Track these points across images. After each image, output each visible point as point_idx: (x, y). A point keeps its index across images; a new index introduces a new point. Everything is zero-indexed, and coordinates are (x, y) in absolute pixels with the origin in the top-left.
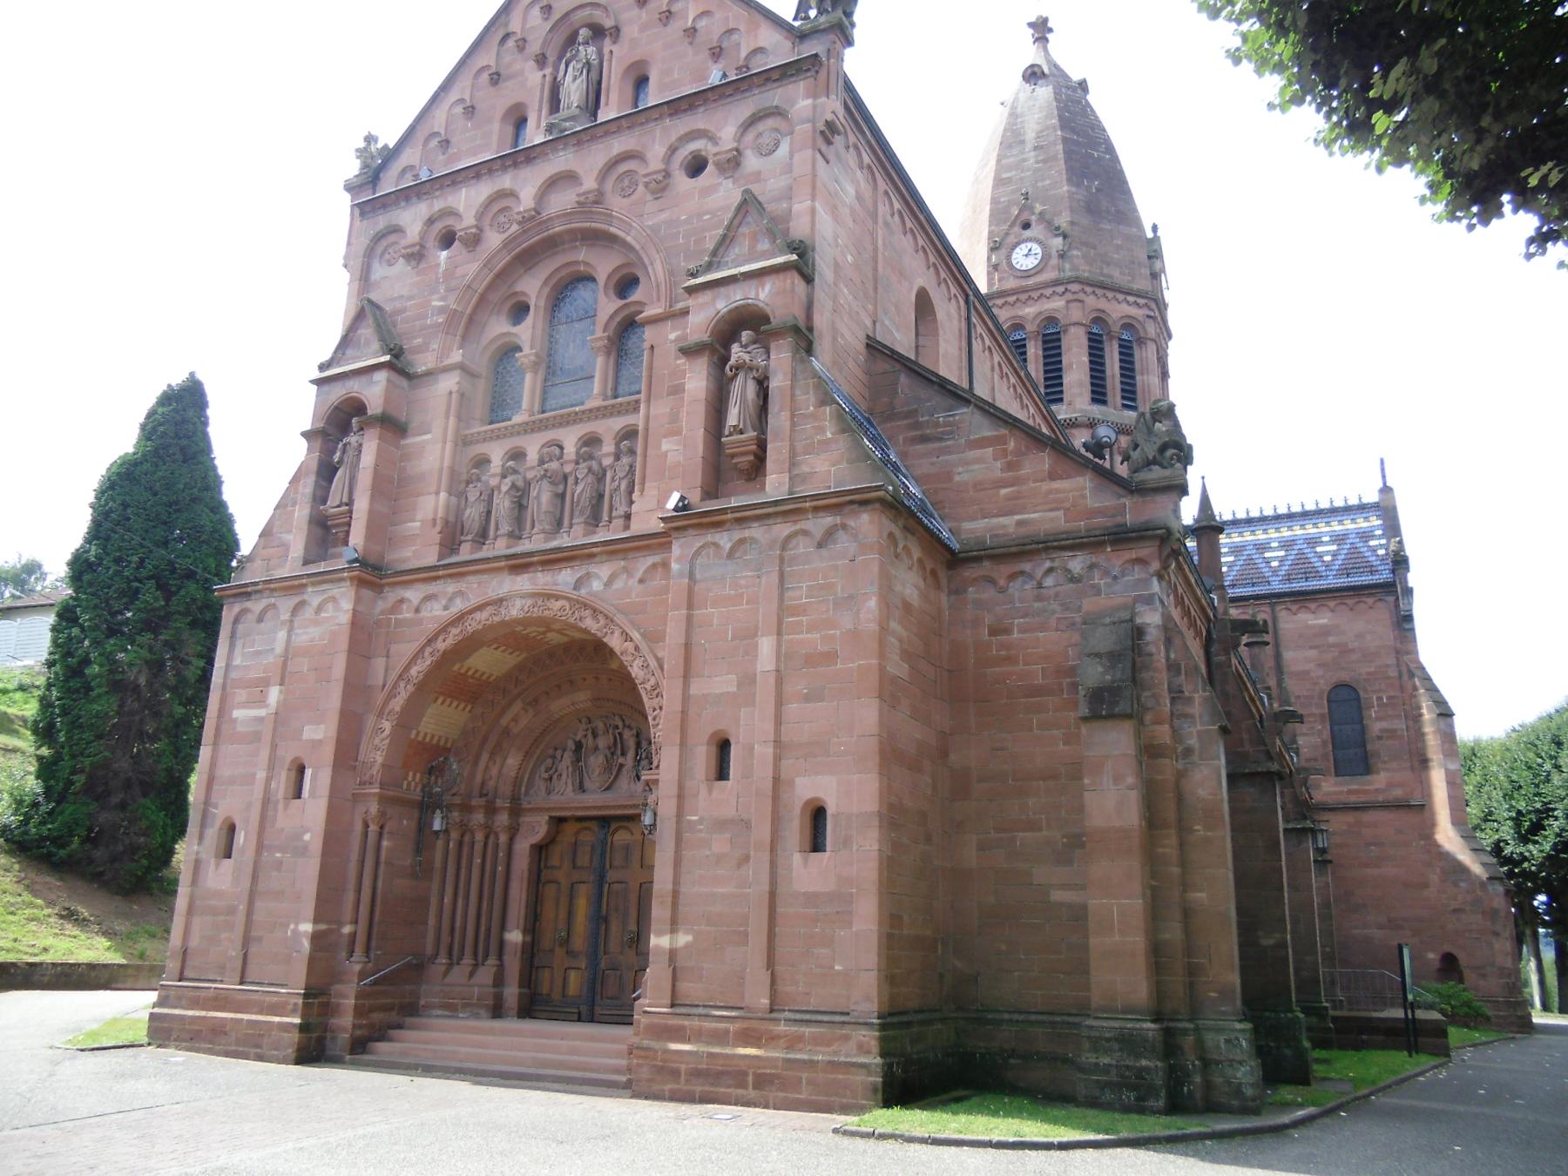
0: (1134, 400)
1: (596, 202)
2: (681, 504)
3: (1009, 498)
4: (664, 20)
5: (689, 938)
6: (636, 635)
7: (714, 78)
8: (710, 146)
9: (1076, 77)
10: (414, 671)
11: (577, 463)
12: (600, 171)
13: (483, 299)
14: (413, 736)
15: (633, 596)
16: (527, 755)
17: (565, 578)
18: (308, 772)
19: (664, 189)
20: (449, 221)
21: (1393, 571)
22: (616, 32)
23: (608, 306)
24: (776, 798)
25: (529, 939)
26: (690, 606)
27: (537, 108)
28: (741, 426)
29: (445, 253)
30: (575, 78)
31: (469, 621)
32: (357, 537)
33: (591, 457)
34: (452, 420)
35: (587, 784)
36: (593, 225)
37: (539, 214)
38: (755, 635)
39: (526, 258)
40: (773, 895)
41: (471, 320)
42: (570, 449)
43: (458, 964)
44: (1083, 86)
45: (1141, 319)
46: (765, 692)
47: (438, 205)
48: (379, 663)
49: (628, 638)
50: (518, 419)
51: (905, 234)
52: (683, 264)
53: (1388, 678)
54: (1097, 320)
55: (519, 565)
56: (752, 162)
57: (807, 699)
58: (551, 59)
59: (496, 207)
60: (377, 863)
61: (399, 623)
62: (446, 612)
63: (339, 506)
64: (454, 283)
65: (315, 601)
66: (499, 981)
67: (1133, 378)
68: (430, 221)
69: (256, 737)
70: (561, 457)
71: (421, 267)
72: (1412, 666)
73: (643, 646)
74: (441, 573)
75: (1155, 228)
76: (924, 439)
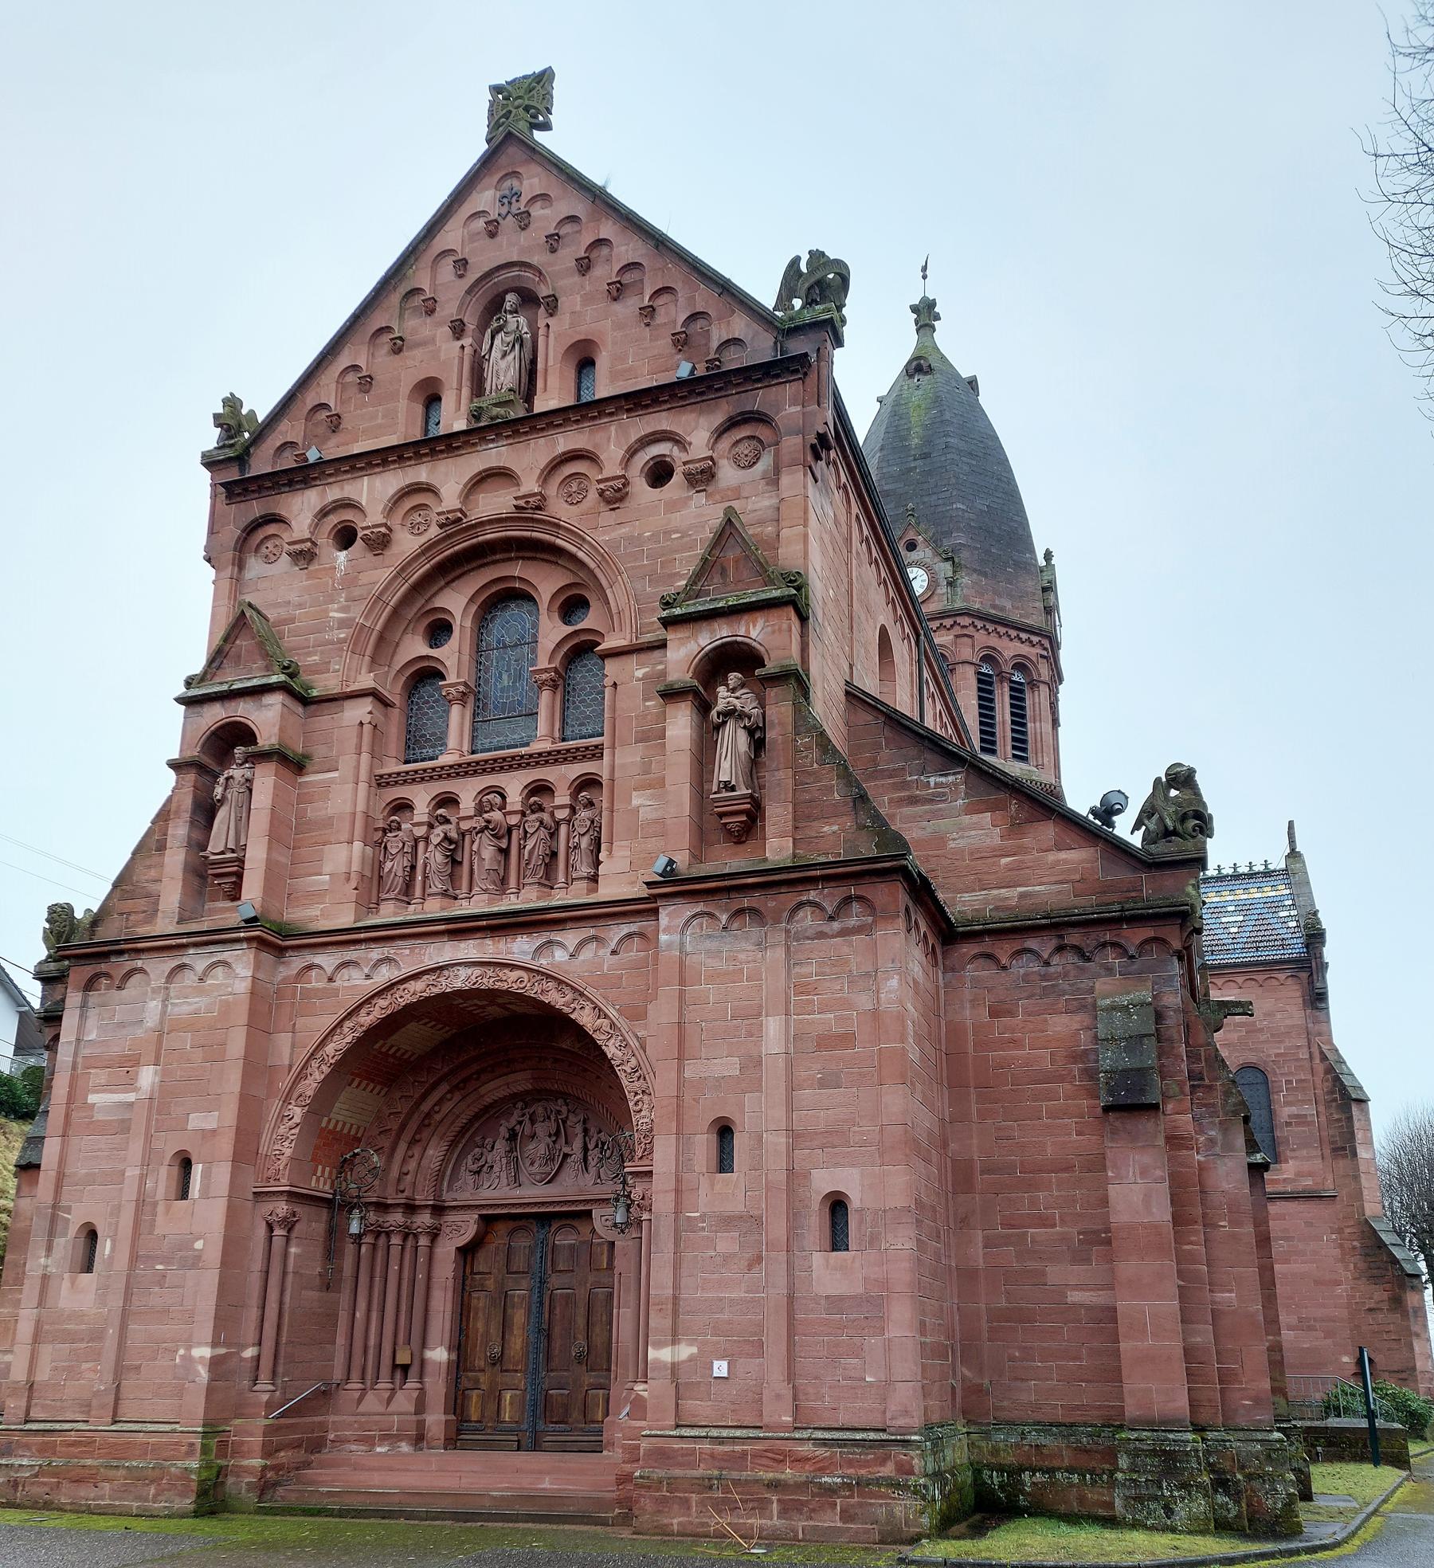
0: (1024, 750)
1: (539, 508)
2: (669, 868)
3: (1010, 868)
4: (615, 293)
5: (694, 1350)
6: (612, 1012)
7: (684, 371)
8: (676, 451)
9: (965, 373)
10: (330, 1049)
11: (524, 814)
12: (543, 471)
13: (396, 613)
14: (323, 1125)
16: (453, 1144)
17: (520, 947)
18: (197, 1170)
19: (621, 499)
20: (348, 515)
21: (1307, 947)
22: (552, 305)
23: (552, 632)
24: (790, 1191)
25: (454, 1357)
26: (682, 982)
27: (455, 385)
28: (733, 783)
29: (342, 556)
30: (505, 355)
31: (400, 993)
32: (252, 889)
33: (541, 809)
34: (365, 757)
35: (522, 1179)
36: (535, 534)
37: (466, 516)
38: (759, 1015)
39: (448, 570)
40: (791, 1299)
41: (381, 638)
42: (515, 799)
43: (401, 1389)
44: (972, 383)
45: (1034, 659)
46: (774, 1075)
47: (333, 493)
48: (284, 1041)
49: (601, 1014)
50: (445, 759)
51: (870, 564)
52: (648, 589)
53: (1298, 1060)
54: (987, 659)
55: (461, 929)
56: (728, 473)
57: (823, 1084)
58: (471, 327)
59: (409, 503)
60: (284, 1273)
61: (307, 994)
62: (369, 982)
63: (222, 853)
64: (357, 592)
65: (200, 965)
66: (420, 1406)
67: (1024, 725)
68: (324, 513)
69: (124, 1127)
70: (502, 808)
71: (311, 568)
72: (1325, 1048)
73: (622, 1023)
75: (1048, 555)
76: (913, 801)
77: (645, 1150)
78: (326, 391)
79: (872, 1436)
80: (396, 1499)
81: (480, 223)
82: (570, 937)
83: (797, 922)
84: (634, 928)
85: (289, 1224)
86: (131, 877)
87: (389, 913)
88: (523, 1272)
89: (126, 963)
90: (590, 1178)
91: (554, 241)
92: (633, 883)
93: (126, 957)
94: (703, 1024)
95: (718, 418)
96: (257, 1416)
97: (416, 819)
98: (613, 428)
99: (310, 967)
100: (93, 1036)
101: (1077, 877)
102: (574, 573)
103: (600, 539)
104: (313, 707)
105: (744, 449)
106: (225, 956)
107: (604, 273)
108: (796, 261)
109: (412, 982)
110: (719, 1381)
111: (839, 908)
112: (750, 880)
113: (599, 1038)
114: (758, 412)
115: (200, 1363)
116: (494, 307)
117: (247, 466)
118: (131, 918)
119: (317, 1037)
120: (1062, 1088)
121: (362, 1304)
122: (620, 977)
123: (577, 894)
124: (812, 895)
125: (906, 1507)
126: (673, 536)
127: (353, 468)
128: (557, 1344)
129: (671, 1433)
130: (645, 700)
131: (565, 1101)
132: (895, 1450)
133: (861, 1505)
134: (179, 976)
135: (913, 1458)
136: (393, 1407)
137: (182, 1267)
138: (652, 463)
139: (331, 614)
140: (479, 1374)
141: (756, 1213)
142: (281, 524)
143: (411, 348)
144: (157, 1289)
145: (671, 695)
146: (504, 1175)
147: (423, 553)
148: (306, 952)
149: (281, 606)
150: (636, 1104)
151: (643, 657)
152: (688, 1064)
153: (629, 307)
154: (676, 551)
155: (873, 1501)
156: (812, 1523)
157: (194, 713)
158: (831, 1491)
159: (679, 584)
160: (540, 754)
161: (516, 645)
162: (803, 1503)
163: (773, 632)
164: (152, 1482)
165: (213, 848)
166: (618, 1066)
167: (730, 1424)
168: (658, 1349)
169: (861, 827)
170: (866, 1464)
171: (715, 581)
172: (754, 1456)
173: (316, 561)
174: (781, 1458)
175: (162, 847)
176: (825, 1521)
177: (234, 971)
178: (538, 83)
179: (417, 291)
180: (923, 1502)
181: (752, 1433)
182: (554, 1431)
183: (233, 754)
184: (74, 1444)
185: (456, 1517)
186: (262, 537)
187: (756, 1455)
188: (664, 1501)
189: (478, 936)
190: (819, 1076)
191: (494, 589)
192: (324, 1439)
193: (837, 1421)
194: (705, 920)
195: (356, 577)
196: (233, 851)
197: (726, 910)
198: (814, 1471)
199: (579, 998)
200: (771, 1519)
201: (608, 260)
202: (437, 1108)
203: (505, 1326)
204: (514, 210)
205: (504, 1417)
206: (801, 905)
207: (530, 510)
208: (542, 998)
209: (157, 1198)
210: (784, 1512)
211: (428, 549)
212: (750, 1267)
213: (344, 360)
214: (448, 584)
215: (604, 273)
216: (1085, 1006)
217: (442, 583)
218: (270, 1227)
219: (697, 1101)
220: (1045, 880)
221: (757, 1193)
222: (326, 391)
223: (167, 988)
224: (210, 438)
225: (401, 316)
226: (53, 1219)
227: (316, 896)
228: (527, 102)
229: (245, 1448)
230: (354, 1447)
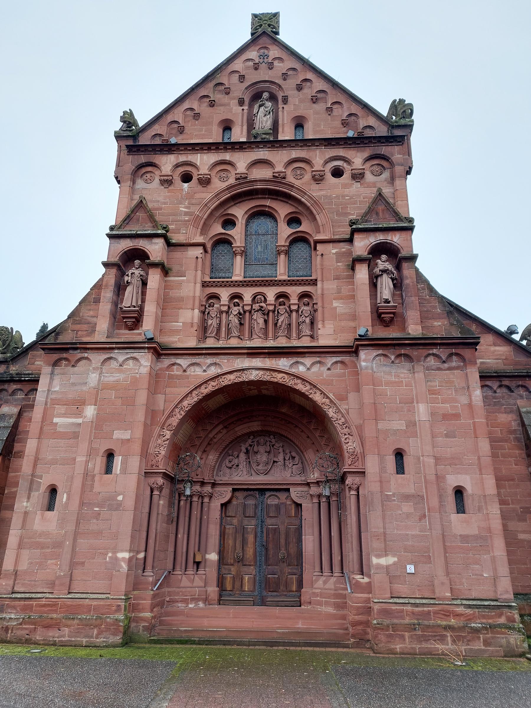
4: (314, 100)
5: (396, 559)
6: (331, 396)
8: (345, 165)
10: (185, 403)
13: (211, 214)
15: (325, 376)
17: (283, 363)
18: (118, 461)
19: (321, 180)
27: (240, 124)
28: (390, 300)
29: (186, 185)
34: (199, 273)
56: (369, 177)
57: (447, 436)
59: (219, 168)
61: (171, 377)
62: (205, 373)
63: (129, 307)
64: (194, 201)
65: (121, 358)
68: (177, 166)
71: (170, 188)
74: (204, 352)
77: (352, 461)
79: (492, 603)
81: (251, 63)
82: (308, 361)
83: (427, 362)
84: (338, 359)
85: (161, 489)
86: (79, 314)
87: (210, 343)
88: (252, 517)
89: (78, 354)
91: (285, 77)
92: (336, 339)
93: (79, 351)
94: (385, 405)
96: (146, 589)
97: (222, 303)
99: (173, 364)
100: (57, 389)
101: (504, 358)
102: (296, 207)
103: (314, 194)
104: (172, 248)
105: (376, 168)
106: (135, 355)
107: (308, 92)
108: (395, 101)
109: (228, 375)
110: (410, 575)
111: (447, 358)
113: (325, 408)
114: (383, 155)
115: (123, 561)
116: (256, 97)
117: (137, 140)
118: (79, 333)
119: (180, 398)
120: (506, 445)
121: (181, 530)
122: (332, 380)
123: (306, 342)
124: (435, 351)
125: (515, 639)
126: (346, 198)
127: (193, 149)
128: (271, 552)
129: (390, 601)
130: (337, 262)
131: (274, 437)
132: (505, 610)
133: (493, 638)
134: (108, 363)
135: (514, 614)
136: (195, 584)
137: (110, 509)
138: (334, 168)
139: (180, 209)
140: (231, 567)
141: (421, 494)
142: (154, 168)
143: (217, 106)
144: (95, 521)
145: (359, 260)
146: (245, 469)
147: (227, 189)
148: (172, 357)
149: (155, 202)
150: (346, 439)
152: (380, 423)
153: (320, 107)
154: (348, 204)
155: (499, 636)
156: (469, 647)
157: (115, 242)
158: (476, 631)
159: (350, 217)
160: (280, 281)
161: (264, 235)
162: (464, 637)
163: (404, 240)
164: (95, 626)
165: (125, 304)
166: (335, 421)
167: (418, 597)
168: (379, 559)
169: (452, 324)
170: (491, 617)
171: (374, 217)
172: (434, 613)
173: (172, 185)
174: (447, 614)
175: (97, 301)
176: (476, 646)
177: (140, 362)
178: (274, 17)
179: (221, 84)
180: (523, 636)
181: (432, 602)
182: (271, 596)
183: (134, 264)
184: (44, 606)
185: (266, 643)
186: (144, 171)
187: (435, 613)
189: (262, 356)
190: (445, 432)
191: (256, 210)
192: (164, 599)
193: (472, 595)
194: (382, 358)
195: (193, 195)
196: (134, 307)
197: (394, 354)
198: (466, 621)
199: (313, 388)
200: (448, 645)
201: (310, 87)
202: (215, 436)
203: (244, 542)
204: (266, 60)
205: (245, 588)
206: (429, 355)
207: (278, 178)
208: (295, 387)
209: (95, 473)
211: (230, 188)
212: (420, 520)
213: (186, 105)
214: (235, 204)
215: (308, 92)
216: (513, 411)
217: (233, 204)
218: (152, 491)
219: (386, 440)
220: (490, 357)
221: (420, 484)
222: (178, 115)
223: (101, 368)
224: (118, 125)
225: (214, 93)
226: (32, 482)
227: (176, 332)
228: (269, 23)
229: (141, 607)
230: (180, 605)
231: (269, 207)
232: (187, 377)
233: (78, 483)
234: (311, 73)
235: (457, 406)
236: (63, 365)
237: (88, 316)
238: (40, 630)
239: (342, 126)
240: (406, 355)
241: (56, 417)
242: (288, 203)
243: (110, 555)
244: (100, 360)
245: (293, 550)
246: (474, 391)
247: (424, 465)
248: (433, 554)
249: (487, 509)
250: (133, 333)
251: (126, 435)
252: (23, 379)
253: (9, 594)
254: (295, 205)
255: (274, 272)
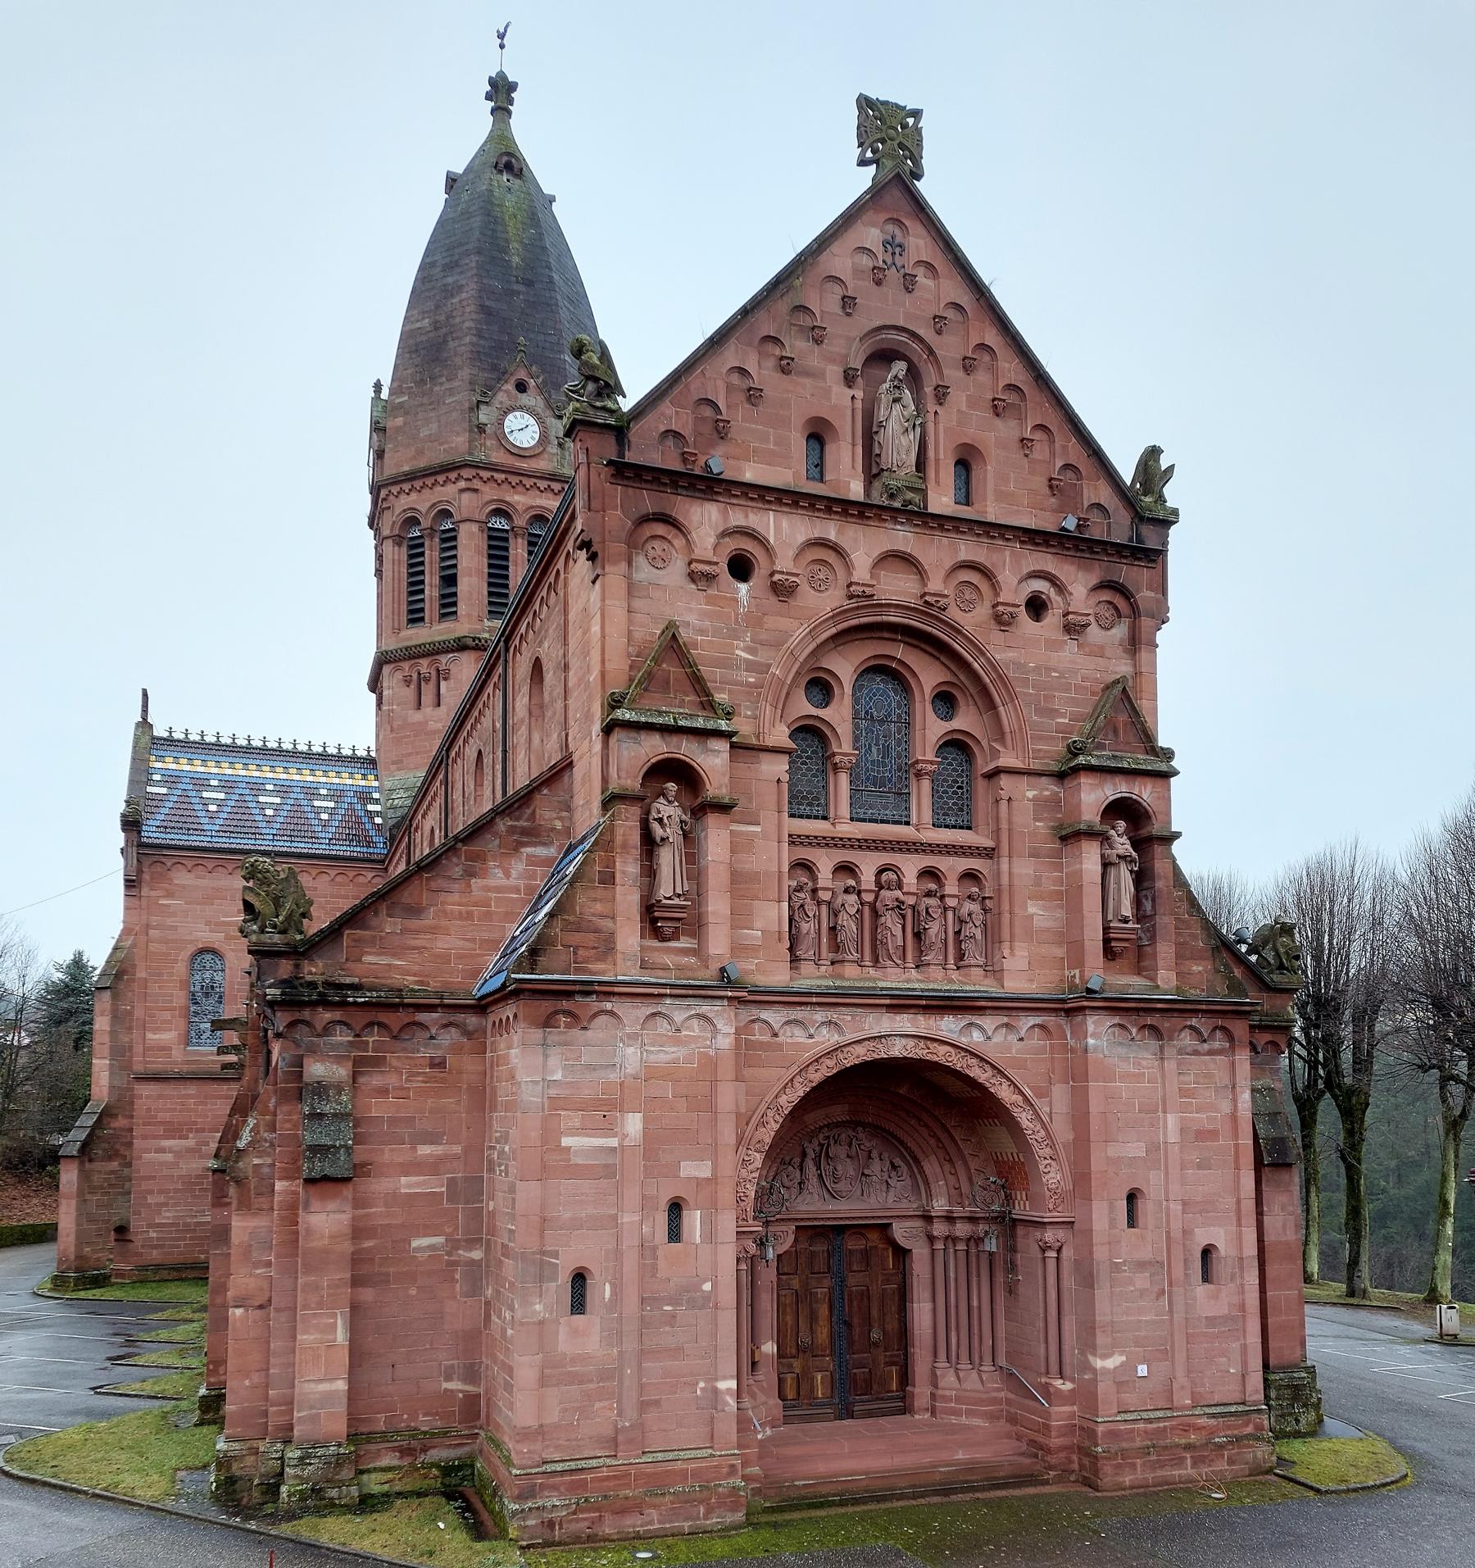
5: (1124, 1358)
6: (1028, 1092)
8: (1052, 593)
10: (783, 1099)
17: (948, 1026)
18: (693, 1221)
19: (1009, 624)
29: (743, 588)
47: (737, 518)
55: (901, 1003)
57: (1200, 1166)
62: (811, 1041)
64: (763, 636)
74: (814, 1000)
78: (715, 383)
80: (864, 1483)
82: (989, 1022)
86: (573, 907)
90: (891, 1198)
95: (1094, 580)
98: (1007, 553)
103: (998, 657)
112: (1159, 1006)
114: (1122, 585)
122: (1026, 1060)
124: (1194, 1022)
128: (857, 1331)
133: (1238, 1454)
139: (737, 652)
141: (1158, 1259)
144: (668, 1329)
151: (1033, 780)
158: (1221, 1446)
163: (1159, 798)
164: (701, 1502)
174: (1186, 1428)
184: (607, 1478)
187: (1172, 1428)
188: (1119, 1466)
194: (1116, 1030)
197: (1135, 1025)
208: (968, 1072)
210: (1195, 1464)
231: (900, 662)
232: (780, 1047)
233: (631, 1263)
234: (994, 331)
235: (1215, 1118)
236: (562, 1025)
237: (593, 915)
238: (608, 1518)
239: (1047, 491)
240: (1152, 1028)
241: (567, 1135)
242: (938, 659)
243: (702, 1384)
244: (638, 1018)
245: (892, 1325)
246: (1242, 1093)
247: (1168, 1216)
248: (1172, 1347)
249: (1242, 1278)
250: (669, 948)
251: (704, 1170)
252: (351, 999)
253: (538, 1466)
254: (952, 666)
255: (904, 813)
